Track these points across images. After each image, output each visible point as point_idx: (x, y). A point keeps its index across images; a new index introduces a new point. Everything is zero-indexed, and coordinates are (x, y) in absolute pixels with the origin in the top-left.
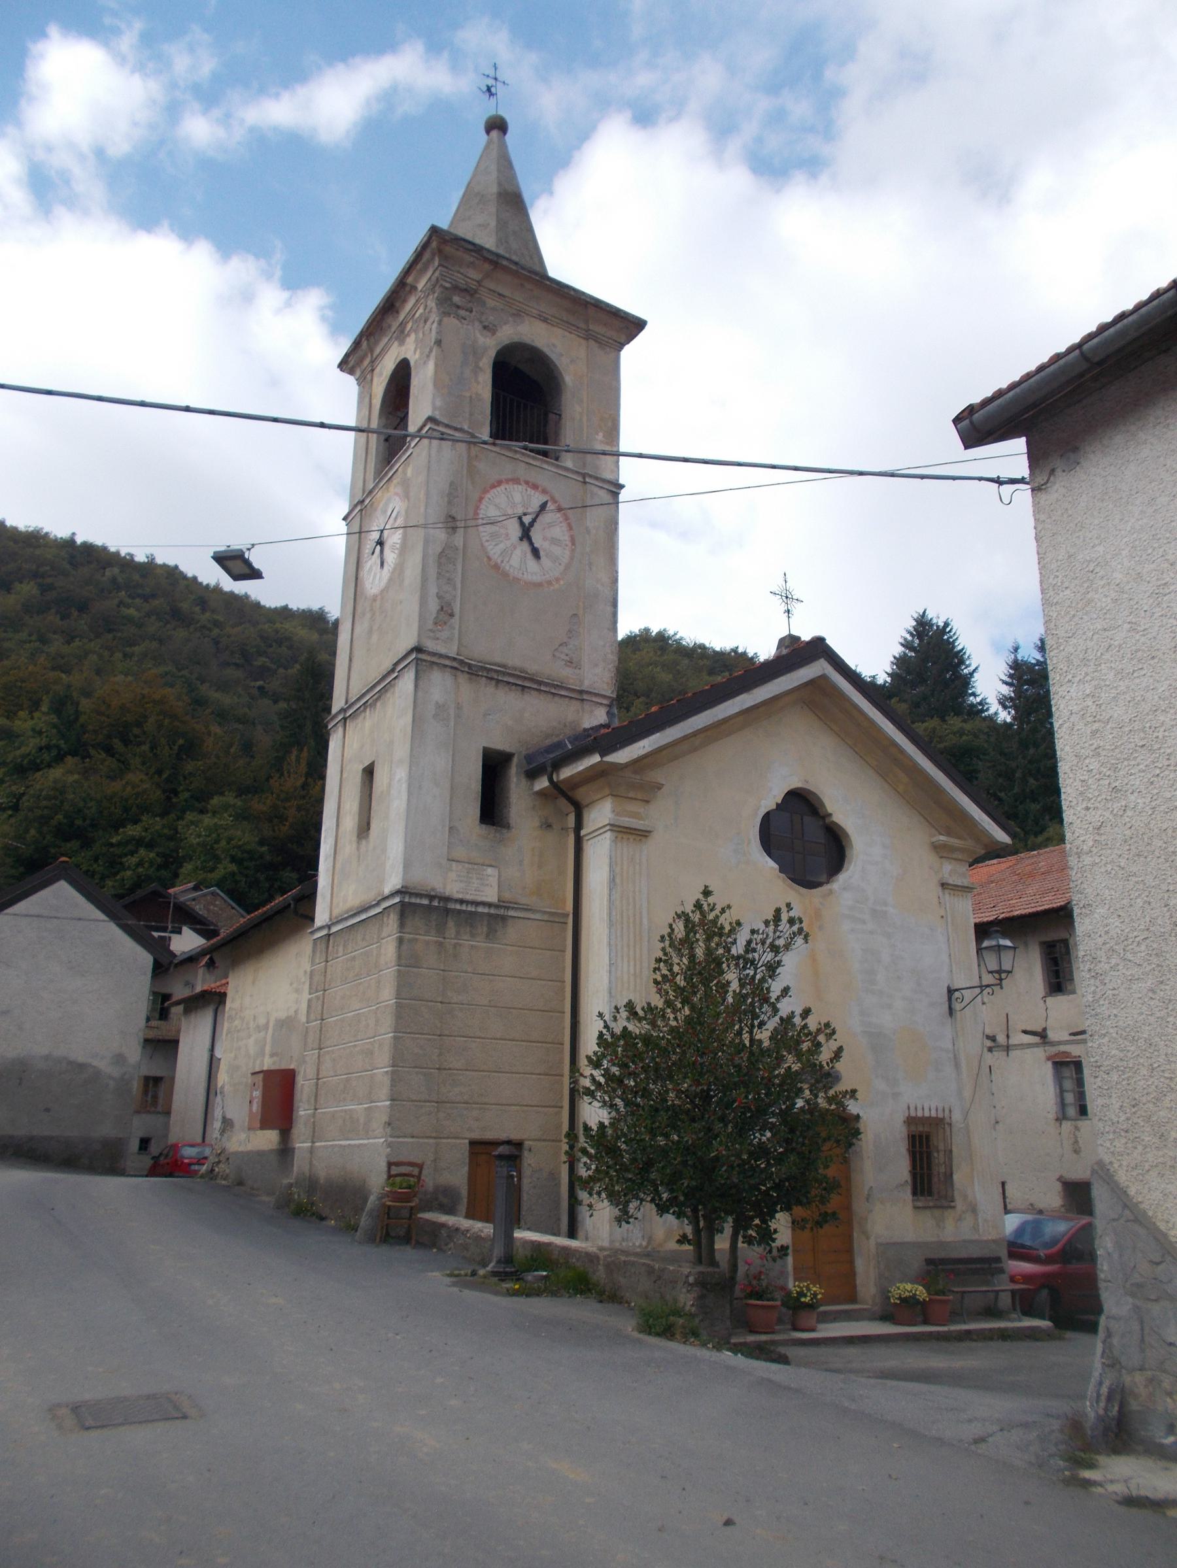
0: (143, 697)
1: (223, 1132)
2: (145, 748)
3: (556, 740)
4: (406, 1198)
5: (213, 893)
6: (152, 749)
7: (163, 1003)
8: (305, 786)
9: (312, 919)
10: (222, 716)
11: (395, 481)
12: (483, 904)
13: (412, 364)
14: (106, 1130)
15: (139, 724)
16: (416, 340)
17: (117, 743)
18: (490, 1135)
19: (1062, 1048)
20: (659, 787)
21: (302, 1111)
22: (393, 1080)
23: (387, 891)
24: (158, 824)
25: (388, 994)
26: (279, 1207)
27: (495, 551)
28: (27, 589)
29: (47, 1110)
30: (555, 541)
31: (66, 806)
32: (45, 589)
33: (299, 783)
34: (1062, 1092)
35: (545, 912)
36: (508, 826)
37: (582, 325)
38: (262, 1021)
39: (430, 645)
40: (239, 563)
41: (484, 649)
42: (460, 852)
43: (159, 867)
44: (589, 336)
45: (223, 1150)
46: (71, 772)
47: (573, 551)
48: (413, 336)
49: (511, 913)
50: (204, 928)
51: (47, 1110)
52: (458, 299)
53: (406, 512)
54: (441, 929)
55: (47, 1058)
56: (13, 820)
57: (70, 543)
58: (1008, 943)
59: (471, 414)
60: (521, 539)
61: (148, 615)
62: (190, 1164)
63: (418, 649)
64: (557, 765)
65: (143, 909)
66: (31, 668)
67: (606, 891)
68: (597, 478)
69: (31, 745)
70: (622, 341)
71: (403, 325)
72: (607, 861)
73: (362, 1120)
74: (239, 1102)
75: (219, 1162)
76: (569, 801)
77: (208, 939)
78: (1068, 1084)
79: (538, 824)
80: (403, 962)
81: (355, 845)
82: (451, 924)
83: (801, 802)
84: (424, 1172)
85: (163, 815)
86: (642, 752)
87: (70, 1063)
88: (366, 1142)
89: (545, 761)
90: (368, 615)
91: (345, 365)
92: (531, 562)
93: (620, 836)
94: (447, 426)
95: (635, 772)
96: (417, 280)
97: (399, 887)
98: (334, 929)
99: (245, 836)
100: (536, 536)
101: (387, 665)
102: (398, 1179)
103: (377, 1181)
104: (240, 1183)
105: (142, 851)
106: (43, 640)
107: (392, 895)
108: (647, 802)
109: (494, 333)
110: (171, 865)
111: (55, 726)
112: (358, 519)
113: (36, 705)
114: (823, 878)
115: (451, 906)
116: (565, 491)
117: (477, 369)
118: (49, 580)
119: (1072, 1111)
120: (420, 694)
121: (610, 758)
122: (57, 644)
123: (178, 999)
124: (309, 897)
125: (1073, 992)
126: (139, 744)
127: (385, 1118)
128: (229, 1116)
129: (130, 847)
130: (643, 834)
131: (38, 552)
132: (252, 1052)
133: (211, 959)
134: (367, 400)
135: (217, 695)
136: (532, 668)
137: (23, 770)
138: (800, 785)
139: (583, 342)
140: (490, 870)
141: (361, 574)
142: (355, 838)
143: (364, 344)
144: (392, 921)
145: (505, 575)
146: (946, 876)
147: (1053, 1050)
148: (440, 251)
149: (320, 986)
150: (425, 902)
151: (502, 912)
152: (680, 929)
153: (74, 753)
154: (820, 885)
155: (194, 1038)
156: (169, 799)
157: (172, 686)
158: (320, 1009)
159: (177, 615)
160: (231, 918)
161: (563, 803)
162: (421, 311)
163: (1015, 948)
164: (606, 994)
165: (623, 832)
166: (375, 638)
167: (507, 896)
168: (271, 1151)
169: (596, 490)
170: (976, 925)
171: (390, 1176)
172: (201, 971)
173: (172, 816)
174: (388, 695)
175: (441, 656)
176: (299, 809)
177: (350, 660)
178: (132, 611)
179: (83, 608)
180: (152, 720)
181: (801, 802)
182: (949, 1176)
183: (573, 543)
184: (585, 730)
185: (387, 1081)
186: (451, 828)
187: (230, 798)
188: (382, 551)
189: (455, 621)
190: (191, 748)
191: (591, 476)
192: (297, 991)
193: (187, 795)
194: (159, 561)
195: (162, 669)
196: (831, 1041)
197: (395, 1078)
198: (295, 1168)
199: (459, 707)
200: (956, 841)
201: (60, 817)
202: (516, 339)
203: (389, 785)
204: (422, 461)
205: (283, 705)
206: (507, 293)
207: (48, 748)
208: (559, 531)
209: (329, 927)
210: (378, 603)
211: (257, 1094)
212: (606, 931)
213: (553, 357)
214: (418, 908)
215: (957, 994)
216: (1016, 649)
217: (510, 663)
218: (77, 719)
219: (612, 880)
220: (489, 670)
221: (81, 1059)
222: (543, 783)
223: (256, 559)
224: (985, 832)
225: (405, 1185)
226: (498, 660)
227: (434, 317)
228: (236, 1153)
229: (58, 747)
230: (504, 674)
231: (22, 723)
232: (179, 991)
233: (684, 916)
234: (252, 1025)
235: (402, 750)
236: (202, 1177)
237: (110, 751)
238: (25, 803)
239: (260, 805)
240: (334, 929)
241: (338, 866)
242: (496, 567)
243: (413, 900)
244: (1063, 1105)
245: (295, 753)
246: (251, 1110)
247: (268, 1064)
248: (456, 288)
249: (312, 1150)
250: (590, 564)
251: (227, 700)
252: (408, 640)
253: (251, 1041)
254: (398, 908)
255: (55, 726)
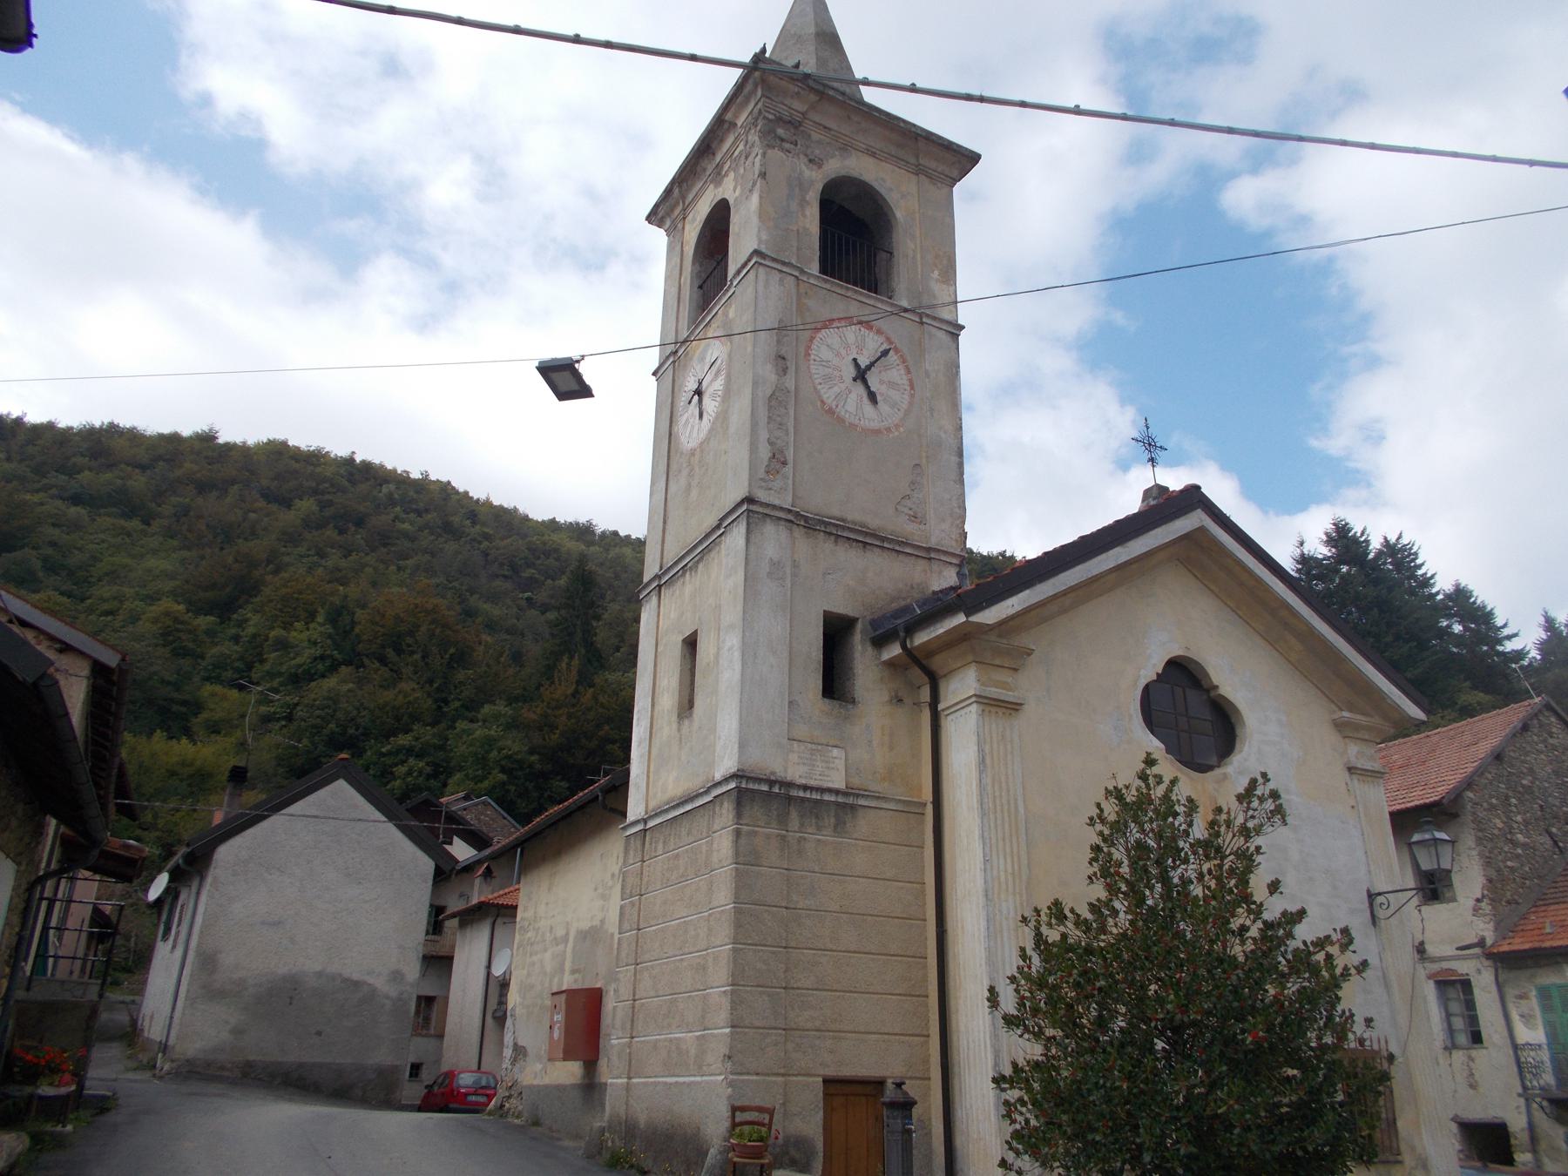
0: (416, 606)
1: (514, 1061)
2: (417, 657)
3: (903, 603)
4: (757, 1154)
5: (484, 803)
6: (423, 657)
7: (437, 915)
8: (575, 694)
9: (624, 815)
10: (491, 626)
11: (714, 325)
12: (830, 790)
13: (731, 202)
14: (382, 1056)
15: (411, 633)
16: (735, 179)
17: (390, 654)
18: (847, 1072)
19: (1445, 965)
20: (1029, 652)
21: (614, 1040)
22: (732, 1002)
23: (718, 777)
24: (427, 734)
25: (723, 897)
26: (590, 1156)
27: (829, 395)
28: (306, 505)
29: (319, 1033)
30: (892, 385)
31: (339, 715)
32: (323, 505)
33: (570, 692)
34: (1448, 1016)
35: (904, 802)
36: (853, 701)
37: (913, 160)
38: (560, 932)
39: (762, 495)
40: (567, 374)
41: (820, 501)
42: (801, 731)
43: (429, 777)
44: (919, 171)
45: (515, 1083)
46: (344, 681)
47: (912, 396)
48: (732, 175)
49: (862, 802)
50: (477, 839)
51: (319, 1033)
52: (783, 130)
53: (730, 355)
54: (783, 821)
55: (319, 974)
56: (285, 731)
57: (350, 461)
58: (1443, 836)
59: (799, 249)
60: (854, 380)
61: (421, 529)
62: (466, 1095)
63: (749, 500)
64: (912, 628)
65: (421, 816)
66: (309, 580)
67: (974, 774)
68: (935, 318)
69: (305, 657)
70: (955, 174)
71: (719, 166)
72: (975, 738)
73: (693, 1052)
74: (533, 1024)
75: (509, 1097)
76: (922, 675)
77: (479, 850)
78: (1455, 1007)
79: (886, 698)
80: (741, 859)
81: (675, 726)
82: (794, 814)
83: (1182, 674)
84: (776, 1117)
85: (433, 724)
86: (1011, 611)
87: (346, 980)
88: (698, 1079)
89: (894, 626)
90: (685, 472)
91: (656, 216)
92: (867, 407)
93: (988, 709)
94: (774, 260)
95: (1000, 636)
96: (736, 116)
97: (734, 770)
98: (651, 824)
99: (514, 745)
100: (872, 379)
101: (711, 521)
102: (747, 1128)
103: (715, 1129)
104: (536, 1123)
105: (412, 761)
106: (322, 555)
107: (726, 780)
108: (1016, 670)
109: (820, 166)
110: (441, 773)
111: (330, 636)
112: (670, 372)
113: (312, 616)
114: (1213, 760)
115: (794, 793)
116: (899, 329)
117: (803, 203)
118: (327, 497)
119: (1462, 1039)
120: (752, 549)
121: (974, 619)
122: (334, 559)
123: (466, 904)
124: (620, 787)
125: (1454, 899)
126: (413, 652)
127: (724, 1050)
128: (520, 1043)
129: (401, 756)
130: (1014, 707)
131: (318, 470)
132: (548, 969)
133: (488, 868)
134: (678, 248)
135: (487, 606)
136: (873, 522)
137: (298, 680)
138: (1181, 653)
139: (914, 177)
140: (835, 752)
141: (675, 429)
142: (674, 718)
143: (676, 191)
144: (726, 812)
145: (841, 420)
146: (1353, 759)
147: (1436, 967)
148: (763, 81)
149: (634, 893)
150: (765, 788)
151: (850, 800)
152: (1111, 810)
153: (348, 663)
154: (1210, 768)
155: (470, 954)
156: (440, 708)
157: (443, 597)
158: (634, 919)
159: (448, 529)
160: (504, 832)
161: (917, 671)
162: (741, 147)
163: (1453, 842)
164: (982, 900)
165: (1000, 707)
166: (694, 493)
167: (856, 781)
168: (573, 1086)
169: (934, 331)
170: (1392, 814)
171: (734, 1125)
172: (477, 881)
173: (443, 725)
174: (713, 554)
175: (774, 507)
176: (570, 716)
177: (665, 522)
178: (406, 526)
179: (360, 522)
180: (423, 629)
181: (1182, 674)
182: (1392, 1123)
183: (912, 388)
184: (934, 593)
185: (725, 1003)
186: (790, 703)
187: (501, 707)
188: (700, 401)
189: (788, 470)
190: (461, 658)
191: (928, 316)
192: (604, 897)
193: (457, 704)
194: (433, 477)
195: (434, 581)
196: (1348, 953)
197: (736, 1001)
198: (608, 1108)
199: (795, 565)
200: (1358, 717)
201: (332, 726)
202: (843, 173)
203: (717, 656)
204: (749, 300)
205: (551, 615)
206: (833, 125)
207: (322, 658)
208: (896, 374)
209: (645, 821)
210: (697, 457)
211: (558, 1017)
212: (978, 821)
213: (883, 191)
214: (757, 795)
215: (1380, 899)
216: (1302, 544)
217: (850, 518)
218: (352, 629)
219: (982, 762)
220: (827, 524)
221: (355, 977)
222: (895, 650)
223: (587, 370)
224: (1397, 708)
225: (755, 1136)
226: (835, 512)
227: (758, 150)
228: (530, 1087)
229: (331, 656)
230: (843, 528)
231: (298, 635)
232: (454, 904)
233: (1117, 794)
234: (548, 936)
235: (732, 613)
236: (490, 1114)
237: (383, 660)
238: (300, 713)
239: (530, 714)
240: (651, 824)
241: (654, 751)
242: (831, 412)
243: (751, 786)
244: (1451, 1031)
245: (566, 659)
246: (551, 1037)
247: (568, 982)
248: (780, 120)
249: (628, 1087)
250: (932, 410)
251: (496, 611)
252: (735, 491)
253: (548, 955)
254: (735, 794)
255: (330, 636)
